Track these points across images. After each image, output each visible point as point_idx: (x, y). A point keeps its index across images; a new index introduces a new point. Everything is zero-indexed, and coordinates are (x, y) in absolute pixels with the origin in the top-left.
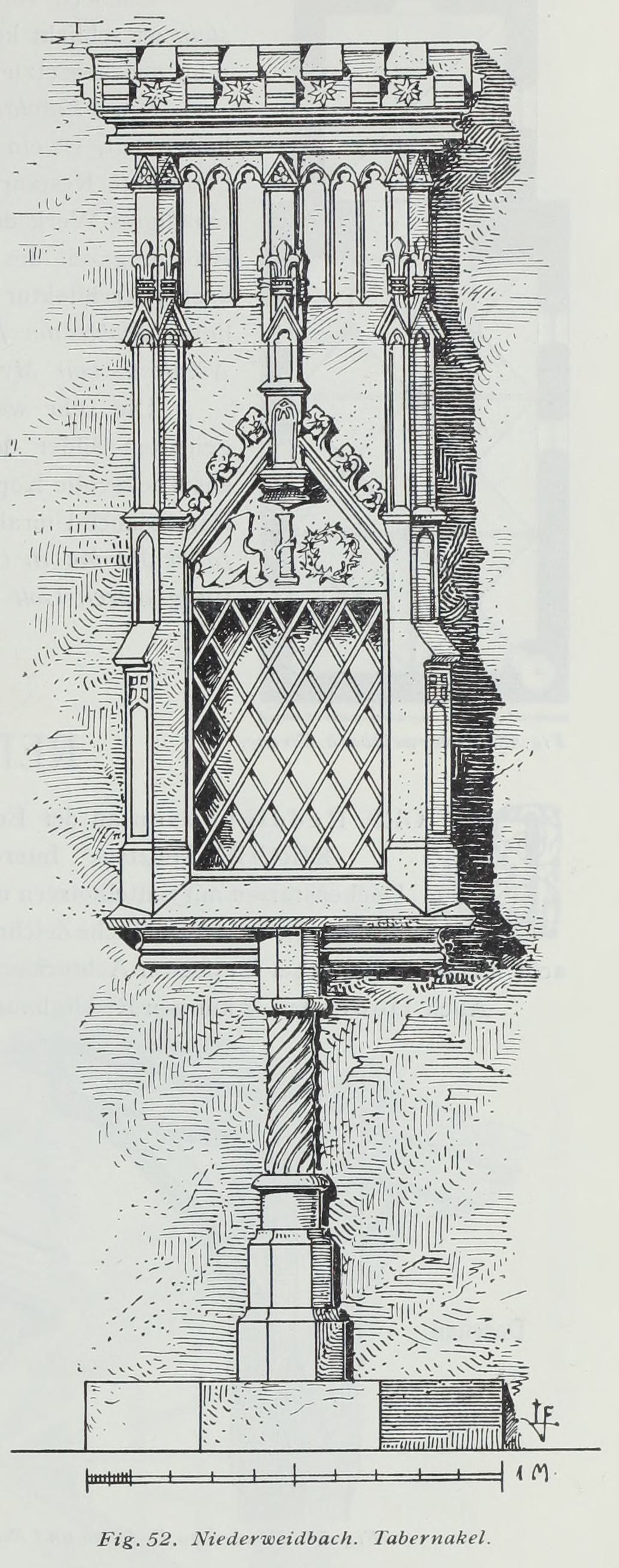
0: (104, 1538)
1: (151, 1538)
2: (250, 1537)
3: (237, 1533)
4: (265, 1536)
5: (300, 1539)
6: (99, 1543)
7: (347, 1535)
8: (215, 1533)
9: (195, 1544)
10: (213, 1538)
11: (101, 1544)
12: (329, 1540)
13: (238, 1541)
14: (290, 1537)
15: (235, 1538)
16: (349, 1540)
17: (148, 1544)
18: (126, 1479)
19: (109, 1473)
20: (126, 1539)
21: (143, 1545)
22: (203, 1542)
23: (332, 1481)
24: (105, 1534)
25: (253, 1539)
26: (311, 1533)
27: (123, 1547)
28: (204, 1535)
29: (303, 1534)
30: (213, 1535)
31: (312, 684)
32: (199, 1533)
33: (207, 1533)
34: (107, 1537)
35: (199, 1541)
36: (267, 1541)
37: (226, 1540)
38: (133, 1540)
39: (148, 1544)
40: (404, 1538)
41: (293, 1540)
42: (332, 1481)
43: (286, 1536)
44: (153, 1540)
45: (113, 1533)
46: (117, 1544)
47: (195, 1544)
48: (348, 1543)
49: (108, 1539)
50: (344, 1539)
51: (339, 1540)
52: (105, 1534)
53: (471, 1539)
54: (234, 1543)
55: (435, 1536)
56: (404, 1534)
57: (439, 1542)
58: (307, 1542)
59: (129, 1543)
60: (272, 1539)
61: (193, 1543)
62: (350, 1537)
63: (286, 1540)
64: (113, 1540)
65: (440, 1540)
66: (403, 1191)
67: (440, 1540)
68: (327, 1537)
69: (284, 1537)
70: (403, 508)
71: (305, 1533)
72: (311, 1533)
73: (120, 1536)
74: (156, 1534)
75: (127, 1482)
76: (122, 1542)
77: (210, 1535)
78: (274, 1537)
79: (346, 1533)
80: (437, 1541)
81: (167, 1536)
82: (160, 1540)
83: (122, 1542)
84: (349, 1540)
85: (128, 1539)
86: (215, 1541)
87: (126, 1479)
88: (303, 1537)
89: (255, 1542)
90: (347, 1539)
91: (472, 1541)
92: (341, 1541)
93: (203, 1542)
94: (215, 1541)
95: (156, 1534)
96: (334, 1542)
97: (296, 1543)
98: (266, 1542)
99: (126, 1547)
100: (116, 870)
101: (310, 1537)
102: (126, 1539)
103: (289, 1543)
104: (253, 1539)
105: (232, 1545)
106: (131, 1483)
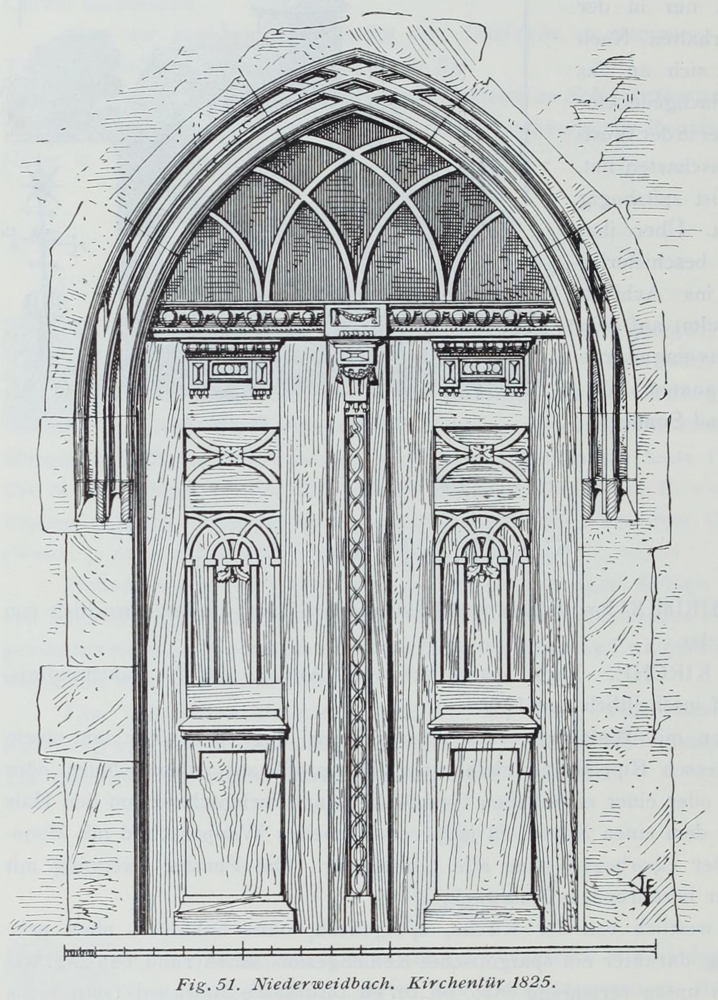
0: (181, 984)
1: (220, 983)
2: (467, 981)
3: (291, 979)
4: (315, 982)
5: (345, 984)
6: (409, 986)
7: (453, 980)
8: (338, 979)
9: (255, 989)
10: (270, 983)
11: (179, 989)
12: (370, 986)
13: (292, 985)
14: (337, 983)
15: (289, 983)
16: (387, 985)
17: (217, 988)
18: (92, 953)
19: (95, 948)
20: (199, 984)
21: (213, 989)
22: (262, 987)
23: (181, 956)
24: (414, 978)
25: (305, 984)
26: (355, 978)
27: (197, 991)
28: (263, 981)
29: (347, 980)
30: (270, 981)
31: (160, 787)
32: (259, 980)
33: (266, 979)
34: (183, 982)
35: (259, 986)
36: (317, 986)
37: (282, 985)
38: (205, 985)
39: (217, 988)
40: (356, 984)
41: (339, 985)
42: (181, 956)
43: (334, 982)
44: (222, 985)
45: (189, 980)
46: (191, 989)
47: (255, 989)
48: (386, 988)
49: (185, 984)
50: (450, 984)
51: (378, 985)
52: (182, 980)
53: (327, 985)
54: (288, 988)
55: (470, 981)
56: (356, 980)
57: (474, 987)
58: (293, 986)
59: (202, 988)
60: (321, 984)
61: (254, 988)
62: (388, 982)
63: (333, 985)
64: (188, 986)
65: (475, 984)
66: (607, 735)
67: (475, 984)
68: (369, 983)
69: (332, 983)
70: (277, 717)
71: (349, 979)
72: (355, 978)
73: (428, 980)
74: (224, 979)
75: (92, 956)
76: (195, 986)
77: (268, 981)
78: (323, 982)
79: (384, 978)
80: (472, 986)
81: (536, 979)
82: (530, 983)
83: (195, 986)
84: (387, 985)
85: (201, 985)
86: (272, 986)
87: (92, 953)
88: (348, 983)
89: (307, 986)
90: (385, 984)
91: (297, 987)
92: (448, 985)
93: (262, 987)
94: (272, 986)
95: (224, 979)
96: (442, 986)
97: (342, 987)
98: (316, 986)
99: (199, 991)
100: (278, 715)
101: (354, 982)
102: (199, 984)
103: (335, 988)
104: (305, 984)
105: (366, 989)
106: (95, 956)
